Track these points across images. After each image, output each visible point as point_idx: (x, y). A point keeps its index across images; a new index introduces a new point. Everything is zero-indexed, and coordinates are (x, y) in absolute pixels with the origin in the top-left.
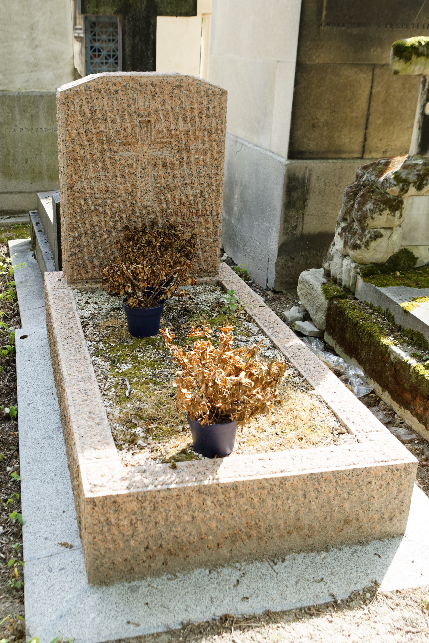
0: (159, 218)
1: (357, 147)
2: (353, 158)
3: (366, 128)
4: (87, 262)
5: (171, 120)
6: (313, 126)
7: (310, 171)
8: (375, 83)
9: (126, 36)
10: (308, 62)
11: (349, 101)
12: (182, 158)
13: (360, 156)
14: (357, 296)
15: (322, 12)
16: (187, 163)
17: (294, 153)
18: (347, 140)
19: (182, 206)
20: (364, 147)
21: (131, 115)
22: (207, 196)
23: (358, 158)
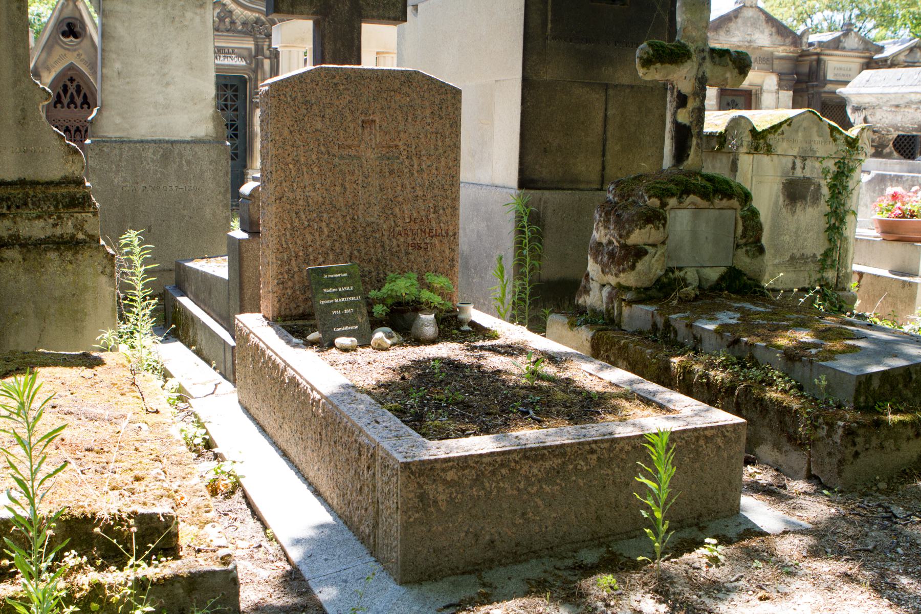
0: (385, 238)
1: (595, 176)
2: (592, 190)
3: (604, 155)
4: (298, 293)
5: (399, 118)
6: (545, 151)
7: (545, 202)
8: (610, 105)
9: (326, 40)
10: (535, 78)
11: (583, 123)
12: (412, 166)
13: (599, 187)
14: (623, 328)
15: (547, 25)
16: (418, 171)
17: (525, 182)
18: (583, 168)
19: (412, 223)
20: (603, 176)
21: (352, 112)
22: (441, 211)
23: (598, 189)
